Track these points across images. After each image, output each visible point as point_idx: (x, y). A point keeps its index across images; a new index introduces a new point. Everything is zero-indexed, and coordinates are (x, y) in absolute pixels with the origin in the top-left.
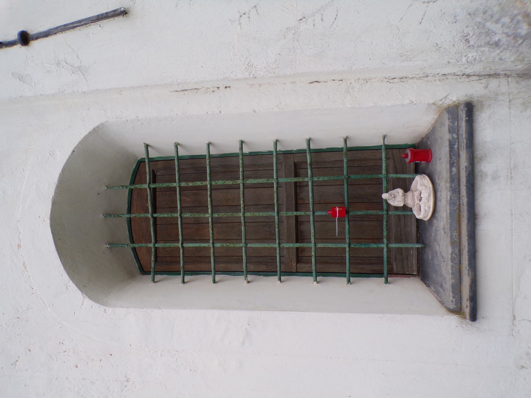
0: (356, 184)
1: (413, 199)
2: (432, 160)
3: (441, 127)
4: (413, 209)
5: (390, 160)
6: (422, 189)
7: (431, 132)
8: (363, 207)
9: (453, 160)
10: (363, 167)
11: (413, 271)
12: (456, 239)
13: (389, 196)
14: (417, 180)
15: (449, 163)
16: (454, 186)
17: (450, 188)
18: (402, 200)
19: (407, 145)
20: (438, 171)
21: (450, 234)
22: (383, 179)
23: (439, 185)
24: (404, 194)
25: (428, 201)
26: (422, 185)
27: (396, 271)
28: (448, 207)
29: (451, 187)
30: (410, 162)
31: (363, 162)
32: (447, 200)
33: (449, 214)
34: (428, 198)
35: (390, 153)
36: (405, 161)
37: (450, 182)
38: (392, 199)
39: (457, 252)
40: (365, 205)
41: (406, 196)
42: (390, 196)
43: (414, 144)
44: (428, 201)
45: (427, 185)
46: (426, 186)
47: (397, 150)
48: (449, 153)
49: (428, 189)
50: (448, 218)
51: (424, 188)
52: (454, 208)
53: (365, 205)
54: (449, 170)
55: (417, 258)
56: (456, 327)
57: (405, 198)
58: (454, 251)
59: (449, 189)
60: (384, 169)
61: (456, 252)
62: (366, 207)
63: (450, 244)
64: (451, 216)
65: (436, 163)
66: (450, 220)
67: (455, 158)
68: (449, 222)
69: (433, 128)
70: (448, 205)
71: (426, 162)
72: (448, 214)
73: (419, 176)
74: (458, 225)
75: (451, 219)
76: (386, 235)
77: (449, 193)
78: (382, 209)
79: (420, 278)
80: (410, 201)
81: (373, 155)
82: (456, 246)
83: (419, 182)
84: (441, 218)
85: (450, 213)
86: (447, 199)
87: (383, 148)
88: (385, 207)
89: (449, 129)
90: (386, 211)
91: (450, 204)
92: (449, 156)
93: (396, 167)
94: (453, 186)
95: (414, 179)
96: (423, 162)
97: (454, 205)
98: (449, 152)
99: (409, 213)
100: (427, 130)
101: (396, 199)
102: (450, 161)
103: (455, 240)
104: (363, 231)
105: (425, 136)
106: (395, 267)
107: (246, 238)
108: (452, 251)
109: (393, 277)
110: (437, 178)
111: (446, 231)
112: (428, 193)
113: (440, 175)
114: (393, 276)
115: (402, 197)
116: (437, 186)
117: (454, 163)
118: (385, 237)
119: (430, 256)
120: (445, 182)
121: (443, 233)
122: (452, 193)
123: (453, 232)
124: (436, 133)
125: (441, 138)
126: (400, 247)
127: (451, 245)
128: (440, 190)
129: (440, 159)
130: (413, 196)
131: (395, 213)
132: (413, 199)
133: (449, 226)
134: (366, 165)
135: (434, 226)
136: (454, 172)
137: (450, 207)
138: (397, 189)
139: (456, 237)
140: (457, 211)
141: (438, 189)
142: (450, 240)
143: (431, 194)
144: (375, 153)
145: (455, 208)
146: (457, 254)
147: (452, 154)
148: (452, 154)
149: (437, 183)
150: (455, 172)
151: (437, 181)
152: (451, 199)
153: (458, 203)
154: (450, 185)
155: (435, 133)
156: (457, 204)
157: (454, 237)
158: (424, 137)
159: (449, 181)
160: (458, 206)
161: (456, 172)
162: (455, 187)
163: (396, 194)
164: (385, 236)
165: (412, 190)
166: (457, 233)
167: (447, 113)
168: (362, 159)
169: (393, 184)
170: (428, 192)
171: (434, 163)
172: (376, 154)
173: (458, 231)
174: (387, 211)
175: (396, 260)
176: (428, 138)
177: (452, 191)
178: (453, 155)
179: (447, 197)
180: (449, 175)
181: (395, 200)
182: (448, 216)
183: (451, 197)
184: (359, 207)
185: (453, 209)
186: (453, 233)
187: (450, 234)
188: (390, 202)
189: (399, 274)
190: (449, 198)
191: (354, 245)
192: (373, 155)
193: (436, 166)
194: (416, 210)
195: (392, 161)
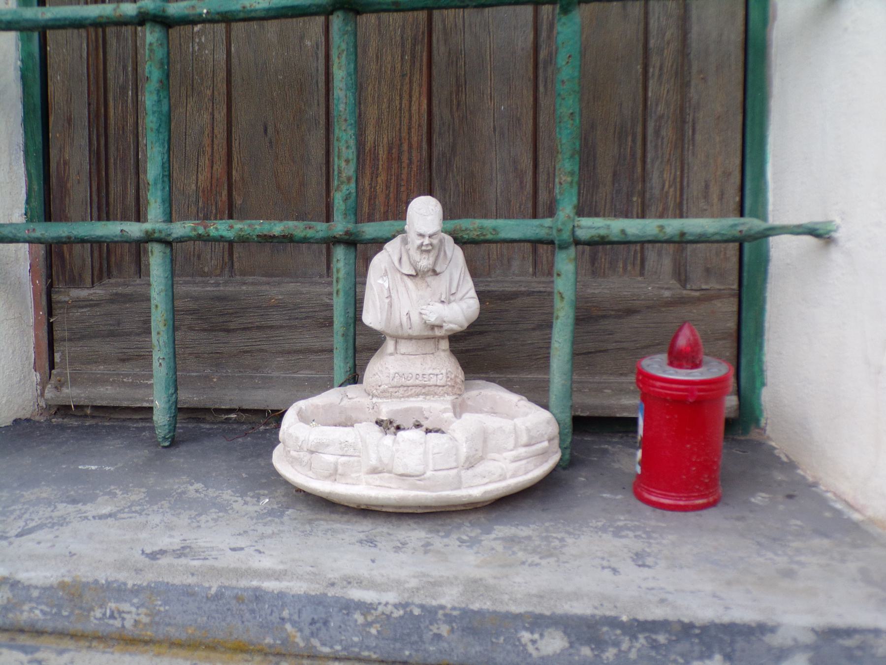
0: (541, 89)
1: (405, 389)
2: (648, 510)
3: (865, 576)
4: (351, 389)
5: (673, 282)
6: (453, 439)
7: (827, 514)
8: (404, 134)
9: (616, 644)
10: (639, 129)
11: (58, 387)
12: (98, 613)
13: (422, 235)
14: (526, 414)
15: (599, 613)
16: (438, 637)
17: (422, 607)
18: (398, 322)
19: (758, 384)
20: (562, 540)
21: (130, 585)
22: (548, 222)
23: (473, 542)
24: (438, 333)
25: (374, 471)
26: (485, 441)
27: (67, 299)
28: (298, 587)
29: (430, 613)
30: (645, 379)
31: (668, 132)
32: (349, 581)
33: (256, 589)
34: (390, 472)
35: (713, 285)
36: (650, 348)
37: (466, 613)
38: (405, 258)
39: (25, 616)
40: (415, 139)
41: (429, 346)
42: (418, 242)
43: (757, 421)
44: (374, 471)
45: (480, 469)
46: (471, 463)
47: (732, 324)
48: (671, 618)
49: (454, 471)
50: (234, 583)
51: (457, 450)
52: (294, 623)
53: (415, 139)
54: (548, 613)
55: (125, 404)
56: (318, 558)
57: (410, 338)
58: (31, 600)
59: (417, 601)
60: (608, 227)
61: (26, 607)
62: (405, 147)
63: (67, 579)
64: (239, 599)
65: (617, 533)
66: (213, 591)
67: (633, 655)
68: (207, 585)
69: (855, 526)
70: (315, 589)
71: (638, 476)
72: (255, 583)
73: (553, 429)
74: (184, 637)
75: (219, 596)
76: (213, 232)
77: (391, 597)
78: (359, 215)
79: (37, 418)
80: (392, 371)
81: (707, 186)
82: (59, 614)
83: (507, 424)
84: (263, 537)
85: (258, 596)
86: (360, 583)
87: (750, 224)
88: (370, 230)
89: (849, 632)
90: (347, 233)
91: (318, 601)
92: (650, 618)
93: (630, 312)
94: (434, 629)
95: (546, 407)
96: (639, 454)
97: (313, 622)
98: (680, 622)
99: (340, 366)
100: (846, 488)
101: (408, 281)
102: (613, 622)
103: (92, 609)
104: (270, 130)
105: (804, 478)
106: (83, 293)
107: (646, 245)
108: (28, 588)
109: (34, 283)
110: (524, 531)
111: (164, 561)
112: (420, 469)
113: (534, 551)
114: (42, 283)
115: (415, 318)
116: (468, 530)
117: (599, 644)
118: (201, 230)
119: (93, 468)
120: (475, 581)
121: (165, 542)
122: (389, 617)
123: (143, 605)
124: (826, 542)
125: (789, 574)
126: (153, 310)
127: (62, 585)
128: (438, 542)
129: (639, 559)
130: (426, 390)
131: (340, 286)
132: (405, 389)
133: (178, 580)
134: (649, 146)
135: (243, 495)
136: (534, 642)
137: (297, 598)
138: (473, 293)
139: (112, 617)
140: (269, 640)
141: (447, 535)
142: (96, 582)
143: (418, 488)
144: (721, 197)
145: (288, 627)
146: (10, 615)
147: (662, 638)
148: (662, 638)
149: (488, 532)
150: (531, 648)
151: (502, 530)
152: (349, 607)
153: (326, 650)
154: (442, 607)
155: (825, 535)
156: (315, 642)
157: (112, 605)
158: (800, 472)
159: (475, 606)
160: (302, 644)
161: (535, 654)
162: (428, 636)
163: (440, 285)
164: (205, 228)
165: (467, 389)
166: (136, 622)
167: (344, 327)
168: (689, 118)
169: (530, 294)
170: (429, 474)
171: (622, 520)
172: (715, 200)
173: (149, 633)
174: (351, 242)
175: (116, 299)
176: (790, 497)
177: (401, 617)
178: (655, 646)
179: (372, 585)
180: (514, 609)
181: (399, 275)
182: (244, 583)
183: (366, 608)
184: (405, 102)
185: (285, 614)
186: (135, 601)
187: (130, 585)
188: (392, 248)
189: (50, 313)
190: (357, 594)
191: (155, 47)
192: (707, 186)
193: (604, 529)
194: (345, 402)
195: (667, 294)
